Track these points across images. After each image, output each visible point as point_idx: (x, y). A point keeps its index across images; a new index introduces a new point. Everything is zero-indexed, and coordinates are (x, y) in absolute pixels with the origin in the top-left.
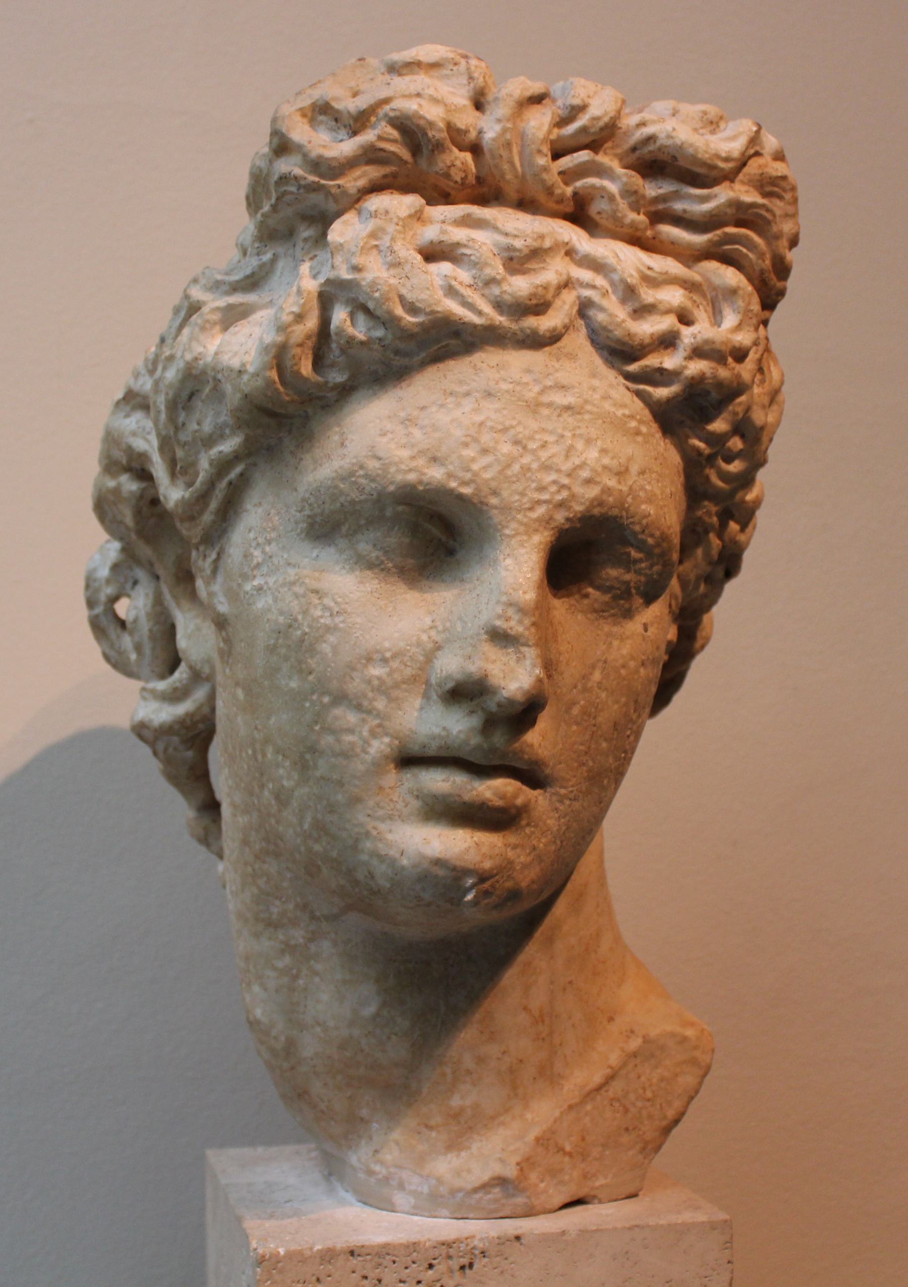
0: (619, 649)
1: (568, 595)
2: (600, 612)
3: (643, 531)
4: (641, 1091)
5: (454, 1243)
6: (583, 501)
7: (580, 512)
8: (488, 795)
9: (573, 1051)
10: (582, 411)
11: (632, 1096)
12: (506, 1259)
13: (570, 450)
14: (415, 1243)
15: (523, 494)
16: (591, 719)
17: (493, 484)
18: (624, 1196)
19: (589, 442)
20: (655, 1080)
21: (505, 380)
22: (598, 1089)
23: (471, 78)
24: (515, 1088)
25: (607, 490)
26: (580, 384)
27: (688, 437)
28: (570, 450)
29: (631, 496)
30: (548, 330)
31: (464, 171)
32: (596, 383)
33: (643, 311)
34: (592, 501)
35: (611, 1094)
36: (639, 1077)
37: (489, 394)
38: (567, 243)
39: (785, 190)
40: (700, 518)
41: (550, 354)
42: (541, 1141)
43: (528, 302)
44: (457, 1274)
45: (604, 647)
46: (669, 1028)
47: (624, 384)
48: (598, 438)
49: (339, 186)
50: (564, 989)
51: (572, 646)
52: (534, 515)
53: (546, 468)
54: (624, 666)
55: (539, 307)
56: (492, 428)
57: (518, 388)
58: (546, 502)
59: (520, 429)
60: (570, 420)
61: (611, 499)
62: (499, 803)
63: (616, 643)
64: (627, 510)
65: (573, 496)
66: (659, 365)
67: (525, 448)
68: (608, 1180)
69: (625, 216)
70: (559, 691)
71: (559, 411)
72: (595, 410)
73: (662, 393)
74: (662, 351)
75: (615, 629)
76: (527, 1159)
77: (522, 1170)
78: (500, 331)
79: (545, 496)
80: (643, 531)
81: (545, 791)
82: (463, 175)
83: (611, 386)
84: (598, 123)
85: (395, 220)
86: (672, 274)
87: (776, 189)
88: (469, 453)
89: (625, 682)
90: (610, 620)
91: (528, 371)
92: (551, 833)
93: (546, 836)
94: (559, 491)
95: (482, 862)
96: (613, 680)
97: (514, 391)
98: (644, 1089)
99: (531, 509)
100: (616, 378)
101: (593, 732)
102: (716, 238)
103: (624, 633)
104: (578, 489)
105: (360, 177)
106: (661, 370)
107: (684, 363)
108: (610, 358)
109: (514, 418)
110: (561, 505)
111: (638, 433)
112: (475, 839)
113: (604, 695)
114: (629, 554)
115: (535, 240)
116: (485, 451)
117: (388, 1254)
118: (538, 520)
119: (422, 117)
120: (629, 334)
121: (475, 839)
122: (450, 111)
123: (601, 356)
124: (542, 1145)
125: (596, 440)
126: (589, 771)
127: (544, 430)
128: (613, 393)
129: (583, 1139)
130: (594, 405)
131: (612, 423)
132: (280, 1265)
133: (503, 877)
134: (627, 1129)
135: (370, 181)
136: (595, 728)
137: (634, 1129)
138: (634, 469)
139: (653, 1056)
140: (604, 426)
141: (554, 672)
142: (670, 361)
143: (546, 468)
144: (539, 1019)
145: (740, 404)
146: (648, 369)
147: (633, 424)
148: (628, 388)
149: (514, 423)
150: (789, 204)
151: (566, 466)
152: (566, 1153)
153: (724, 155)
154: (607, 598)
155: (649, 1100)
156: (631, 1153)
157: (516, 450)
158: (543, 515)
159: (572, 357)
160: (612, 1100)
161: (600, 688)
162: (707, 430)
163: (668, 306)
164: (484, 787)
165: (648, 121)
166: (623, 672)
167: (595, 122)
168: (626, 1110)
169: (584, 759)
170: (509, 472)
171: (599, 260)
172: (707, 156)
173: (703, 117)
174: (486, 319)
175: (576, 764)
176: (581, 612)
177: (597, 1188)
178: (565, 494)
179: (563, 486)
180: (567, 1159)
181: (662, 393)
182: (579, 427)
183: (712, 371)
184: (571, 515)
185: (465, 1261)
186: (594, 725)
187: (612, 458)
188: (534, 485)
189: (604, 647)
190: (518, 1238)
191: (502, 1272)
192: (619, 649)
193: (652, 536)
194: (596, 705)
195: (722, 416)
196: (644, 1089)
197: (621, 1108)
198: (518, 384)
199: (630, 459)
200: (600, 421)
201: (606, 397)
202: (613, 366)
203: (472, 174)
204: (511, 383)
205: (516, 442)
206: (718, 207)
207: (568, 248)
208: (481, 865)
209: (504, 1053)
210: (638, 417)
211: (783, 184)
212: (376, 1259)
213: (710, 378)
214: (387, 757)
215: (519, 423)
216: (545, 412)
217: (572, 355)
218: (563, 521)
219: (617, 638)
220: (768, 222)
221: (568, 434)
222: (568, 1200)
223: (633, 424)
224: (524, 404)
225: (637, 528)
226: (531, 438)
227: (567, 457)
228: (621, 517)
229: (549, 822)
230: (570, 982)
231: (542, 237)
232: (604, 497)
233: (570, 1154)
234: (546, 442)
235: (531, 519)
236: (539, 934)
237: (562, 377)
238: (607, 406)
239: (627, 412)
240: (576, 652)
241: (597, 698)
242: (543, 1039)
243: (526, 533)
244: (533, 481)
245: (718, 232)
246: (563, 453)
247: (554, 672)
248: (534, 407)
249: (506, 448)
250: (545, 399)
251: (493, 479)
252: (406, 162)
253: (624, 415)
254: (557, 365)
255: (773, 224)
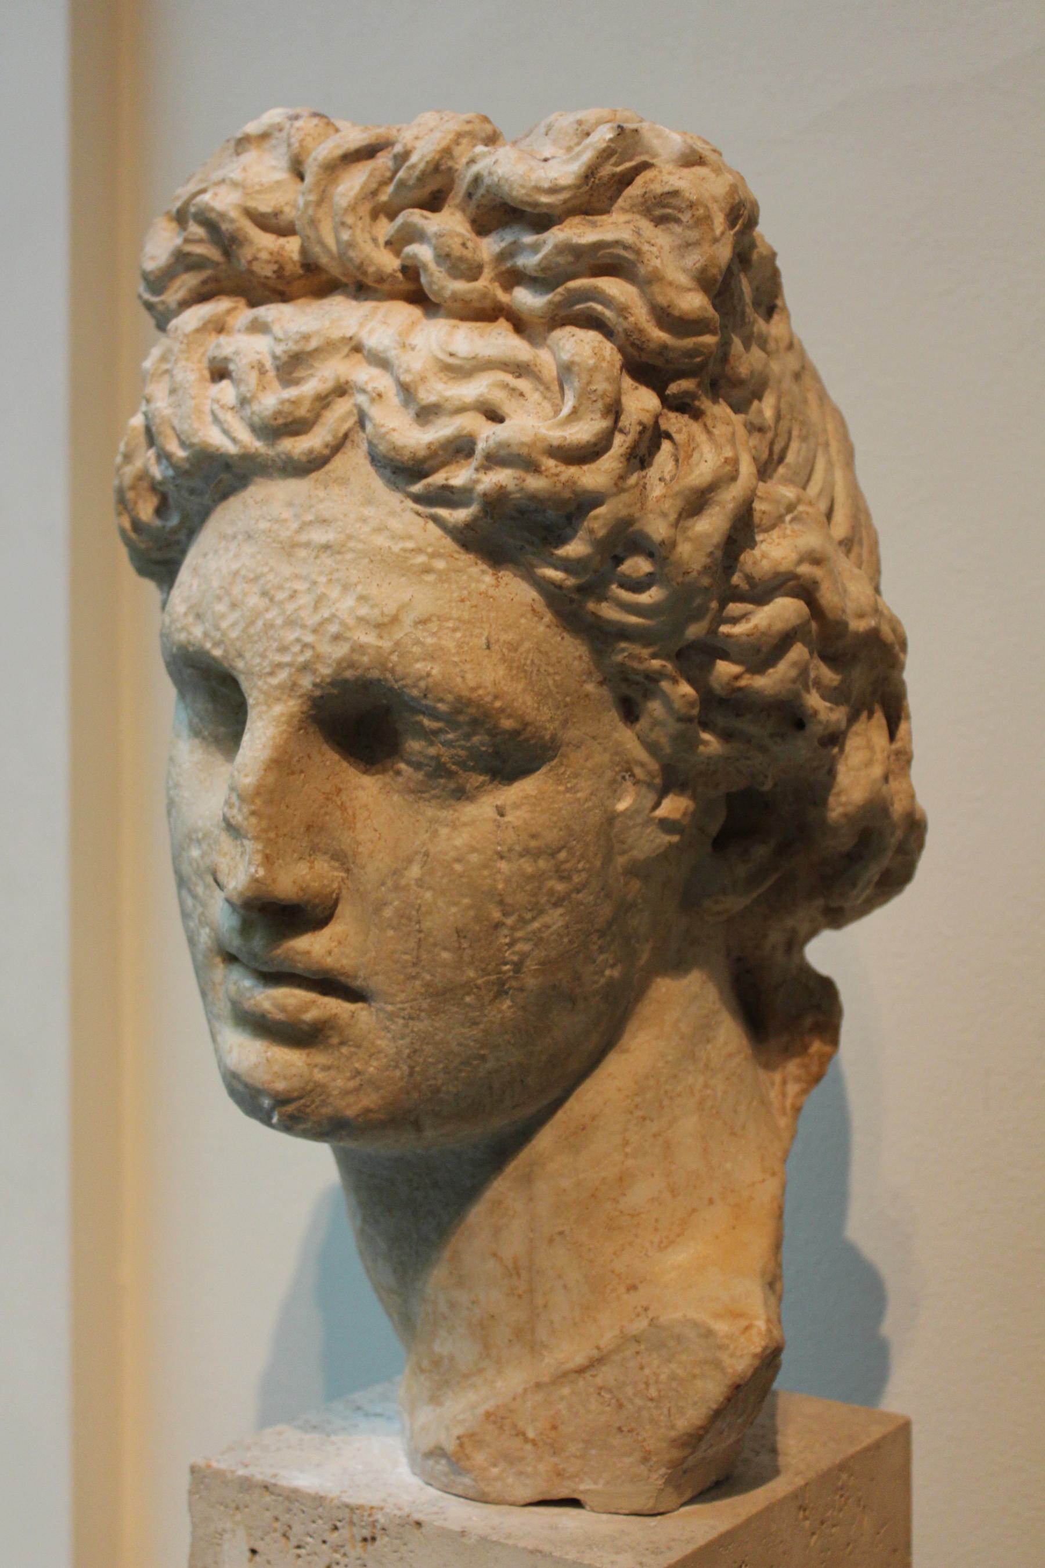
0: (449, 839)
1: (384, 771)
2: (418, 792)
3: (425, 696)
4: (642, 1386)
5: (357, 1509)
6: (329, 662)
7: (328, 676)
8: (267, 1005)
9: (564, 1318)
10: (343, 550)
11: (629, 1390)
12: (405, 1544)
13: (319, 602)
14: (321, 1497)
15: (263, 656)
16: (413, 924)
17: (238, 644)
18: (627, 1512)
19: (346, 587)
20: (663, 1377)
21: (264, 518)
22: (581, 1371)
23: (289, 145)
24: (487, 1346)
25: (360, 648)
26: (345, 515)
27: (533, 566)
28: (319, 602)
29: (396, 653)
30: (303, 453)
31: (276, 262)
32: (369, 511)
33: (426, 414)
34: (339, 663)
35: (599, 1380)
36: (642, 1368)
37: (249, 537)
38: (351, 338)
39: (680, 211)
40: (622, 664)
41: (317, 480)
42: (493, 1418)
43: (275, 423)
44: (360, 1545)
45: (426, 836)
46: (693, 1315)
47: (412, 509)
48: (359, 582)
49: (163, 302)
50: (551, 1241)
51: (380, 834)
52: (274, 681)
53: (291, 623)
54: (458, 860)
55: (296, 427)
56: (244, 577)
57: (276, 527)
58: (289, 665)
59: (270, 577)
60: (327, 560)
61: (365, 659)
62: (280, 1016)
63: (444, 831)
64: (392, 671)
65: (318, 657)
66: (444, 482)
67: (272, 599)
68: (599, 1487)
69: (443, 288)
70: (362, 888)
71: (316, 551)
72: (360, 546)
73: (460, 515)
74: (463, 461)
75: (445, 814)
76: (472, 1435)
77: (461, 1445)
78: (259, 460)
79: (287, 658)
80: (425, 696)
81: (370, 1005)
82: (275, 267)
83: (392, 513)
84: (414, 172)
85: (181, 338)
86: (483, 357)
87: (669, 211)
88: (221, 608)
89: (464, 880)
90: (434, 802)
91: (290, 504)
92: (386, 1056)
93: (378, 1059)
94: (302, 651)
95: (273, 1082)
96: (443, 877)
97: (270, 531)
98: (647, 1384)
99: (272, 674)
100: (402, 502)
101: (420, 940)
102: (558, 298)
103: (458, 819)
104: (325, 648)
105: (180, 287)
106: (446, 488)
107: (475, 476)
108: (393, 477)
109: (267, 564)
110: (305, 668)
111: (427, 570)
112: (269, 1054)
113: (428, 895)
114: (420, 723)
115: (296, 342)
116: (234, 606)
117: (298, 1501)
118: (281, 687)
119: (212, 209)
120: (394, 448)
121: (269, 1054)
122: (248, 194)
123: (382, 476)
124: (494, 1422)
125: (356, 585)
126: (427, 985)
127: (297, 577)
128: (395, 524)
129: (554, 1428)
130: (360, 541)
131: (383, 561)
132: (206, 1480)
133: (313, 1101)
134: (620, 1429)
135: (190, 290)
136: (422, 935)
137: (631, 1431)
138: (408, 620)
139: (663, 1345)
140: (371, 566)
141: (352, 866)
142: (459, 476)
143: (291, 623)
144: (514, 1271)
145: (596, 518)
146: (431, 489)
147: (421, 559)
148: (418, 514)
149: (266, 569)
150: (689, 227)
151: (313, 620)
152: (526, 1440)
153: (546, 185)
154: (420, 776)
155: (651, 1400)
156: (628, 1460)
157: (263, 603)
158: (285, 681)
159: (343, 481)
160: (601, 1388)
161: (421, 886)
162: (555, 555)
163: (457, 403)
164: (263, 996)
165: (478, 155)
166: (458, 867)
167: (411, 172)
168: (620, 1406)
169: (413, 971)
170: (252, 630)
171: (381, 355)
172: (523, 191)
173: (577, 130)
174: (240, 447)
175: (401, 977)
176: (398, 791)
177: (582, 1492)
178: (308, 654)
179: (305, 646)
180: (529, 1447)
181: (460, 515)
182: (337, 570)
183: (516, 482)
184: (318, 680)
185: (366, 1533)
186: (420, 931)
187: (373, 607)
188: (275, 645)
189: (426, 836)
190: (418, 1524)
191: (401, 1558)
192: (449, 839)
193: (441, 700)
194: (417, 907)
195: (579, 535)
196: (647, 1384)
197: (613, 1401)
198: (277, 521)
199: (403, 607)
200: (367, 560)
201: (379, 530)
202: (397, 488)
203: (294, 262)
204: (269, 521)
205: (264, 594)
206: (545, 257)
207: (353, 343)
208: (272, 1085)
209: (473, 1303)
210: (430, 550)
211: (674, 201)
212: (286, 1503)
213: (517, 492)
214: (211, 950)
215: (271, 570)
216: (302, 553)
217: (343, 479)
218: (310, 687)
219: (447, 825)
220: (633, 264)
221: (323, 579)
222: (540, 1498)
223: (421, 559)
224: (279, 546)
225: (415, 692)
226: (280, 587)
227: (316, 608)
228: (386, 680)
229: (379, 1042)
230: (561, 1233)
231: (306, 337)
232: (355, 657)
233: (534, 1442)
234: (295, 591)
235: (271, 686)
236: (514, 1167)
237: (325, 509)
238: (381, 541)
239: (410, 545)
240: (386, 841)
241: (417, 898)
242: (520, 1296)
243: (266, 703)
244: (275, 640)
245: (560, 290)
246: (313, 604)
247: (352, 866)
248: (290, 549)
249: (254, 601)
250: (303, 538)
251: (238, 639)
252: (218, 264)
253: (405, 550)
254: (322, 494)
255: (639, 265)
